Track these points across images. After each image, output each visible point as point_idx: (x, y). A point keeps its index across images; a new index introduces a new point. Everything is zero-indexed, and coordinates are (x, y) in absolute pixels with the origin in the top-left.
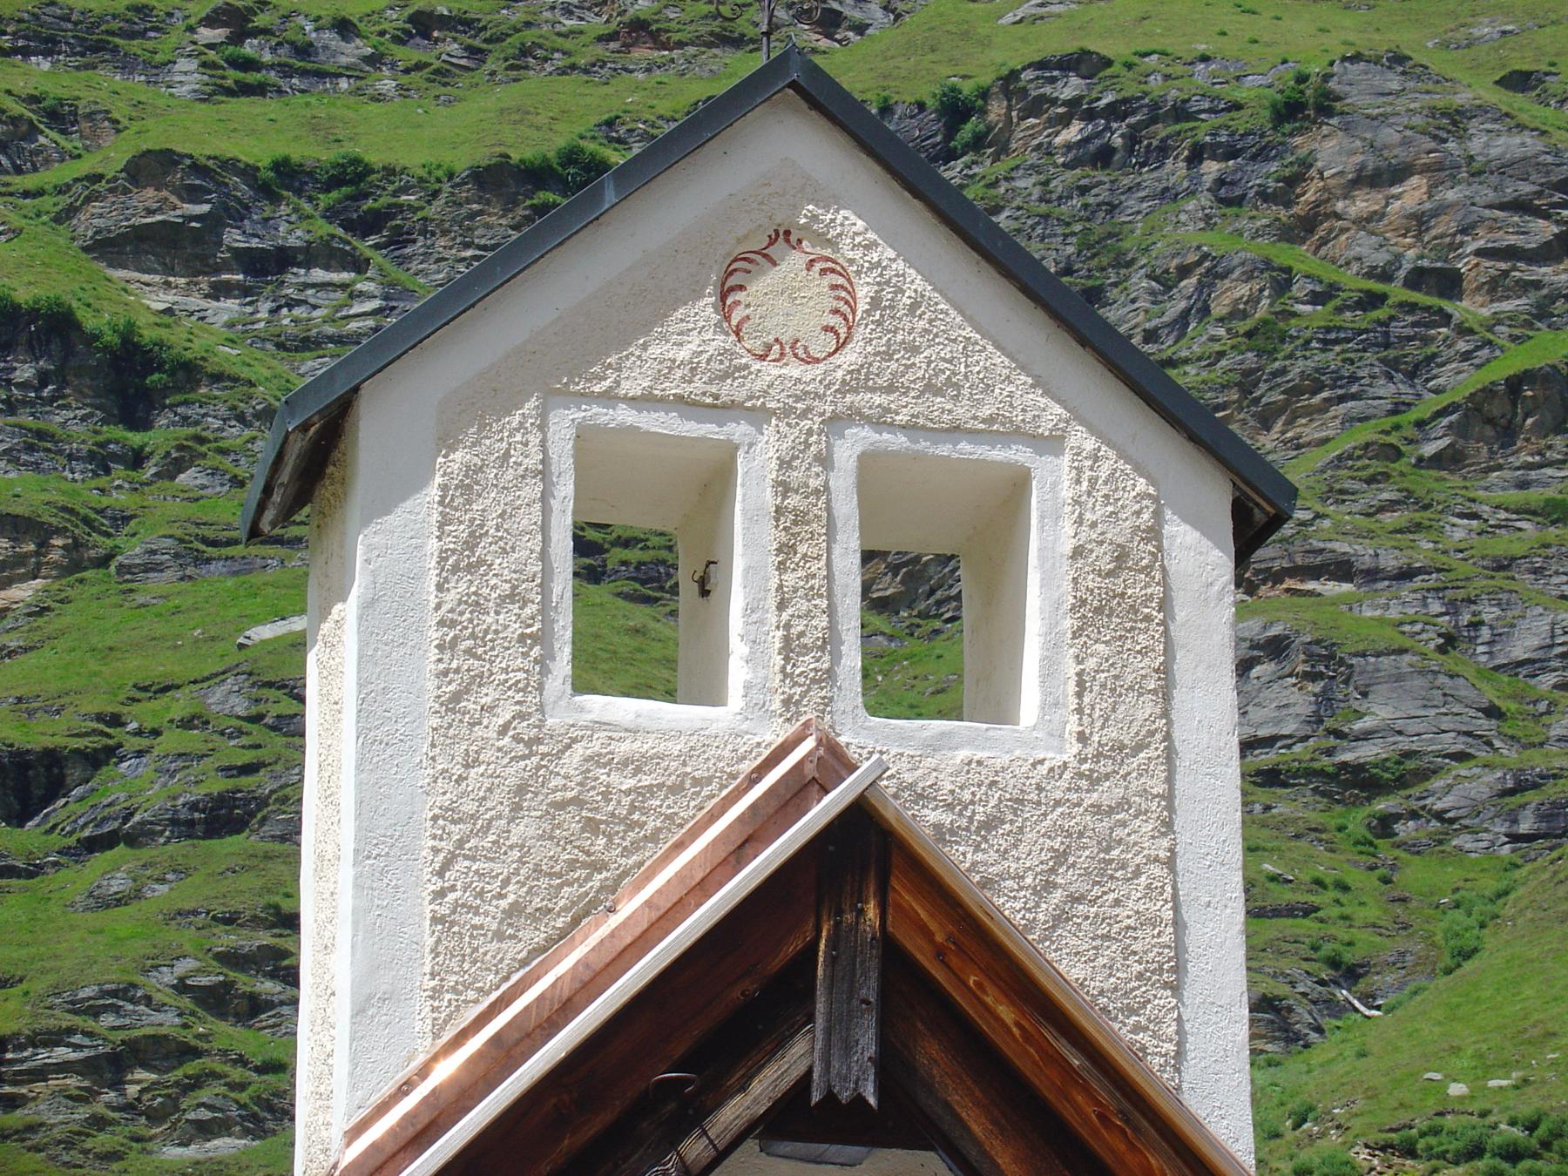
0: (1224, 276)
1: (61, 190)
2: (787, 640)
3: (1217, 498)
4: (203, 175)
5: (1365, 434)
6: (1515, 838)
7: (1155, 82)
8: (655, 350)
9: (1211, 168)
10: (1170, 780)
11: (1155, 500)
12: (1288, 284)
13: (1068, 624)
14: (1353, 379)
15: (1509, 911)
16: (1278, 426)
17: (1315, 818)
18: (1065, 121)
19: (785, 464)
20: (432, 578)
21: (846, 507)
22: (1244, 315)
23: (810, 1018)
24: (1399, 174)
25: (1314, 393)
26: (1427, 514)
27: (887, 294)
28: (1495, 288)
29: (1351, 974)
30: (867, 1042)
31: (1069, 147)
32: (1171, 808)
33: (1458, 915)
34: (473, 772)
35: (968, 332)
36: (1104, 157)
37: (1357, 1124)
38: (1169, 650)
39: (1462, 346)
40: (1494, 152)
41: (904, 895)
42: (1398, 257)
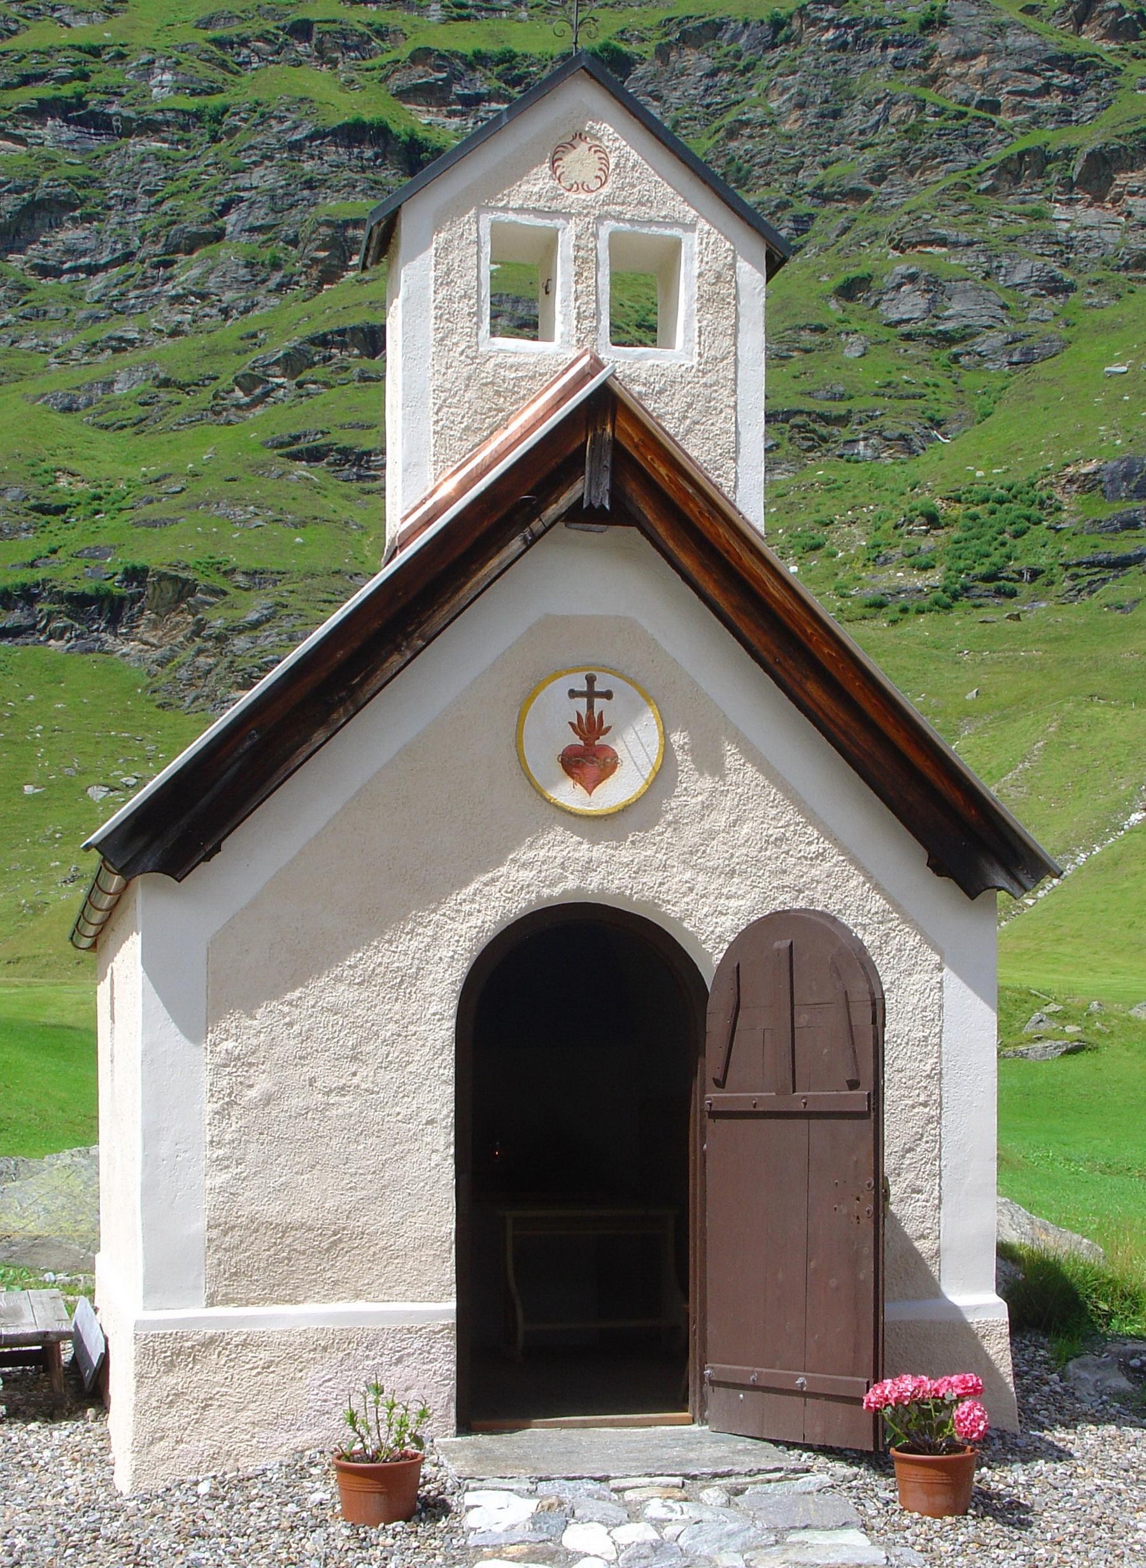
0: (895, 104)
1: (383, 67)
2: (578, 313)
3: (759, 252)
4: (444, 59)
5: (955, 178)
6: (1011, 364)
7: (868, 10)
8: (524, 188)
9: (891, 52)
10: (736, 373)
11: (734, 251)
12: (924, 107)
13: (696, 306)
14: (951, 152)
15: (1006, 396)
16: (917, 175)
17: (926, 355)
18: (827, 29)
19: (578, 237)
20: (432, 289)
21: (604, 256)
22: (904, 122)
23: (583, 473)
24: (975, 55)
25: (933, 159)
26: (981, 216)
27: (622, 161)
28: (1015, 109)
29: (938, 424)
30: (606, 484)
31: (828, 41)
32: (736, 385)
33: (985, 398)
34: (450, 371)
35: (657, 178)
36: (844, 46)
37: (937, 489)
38: (737, 318)
39: (999, 137)
40: (1018, 44)
41: (622, 422)
42: (973, 95)
